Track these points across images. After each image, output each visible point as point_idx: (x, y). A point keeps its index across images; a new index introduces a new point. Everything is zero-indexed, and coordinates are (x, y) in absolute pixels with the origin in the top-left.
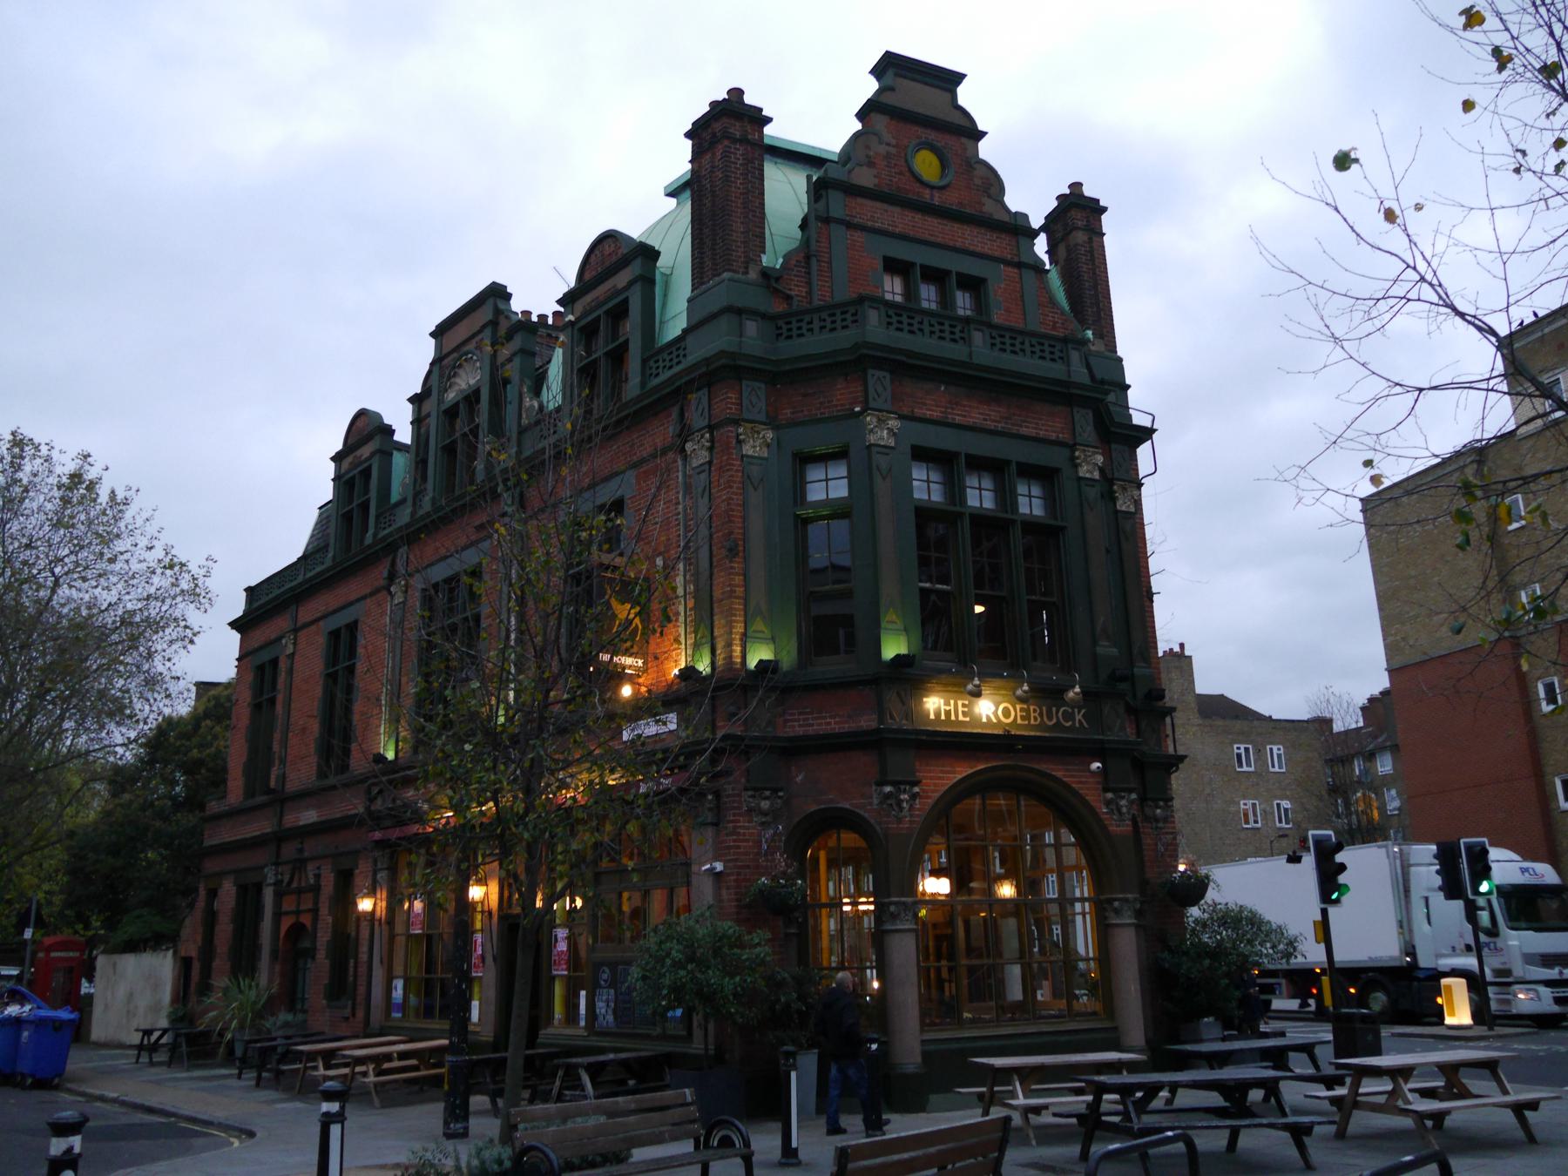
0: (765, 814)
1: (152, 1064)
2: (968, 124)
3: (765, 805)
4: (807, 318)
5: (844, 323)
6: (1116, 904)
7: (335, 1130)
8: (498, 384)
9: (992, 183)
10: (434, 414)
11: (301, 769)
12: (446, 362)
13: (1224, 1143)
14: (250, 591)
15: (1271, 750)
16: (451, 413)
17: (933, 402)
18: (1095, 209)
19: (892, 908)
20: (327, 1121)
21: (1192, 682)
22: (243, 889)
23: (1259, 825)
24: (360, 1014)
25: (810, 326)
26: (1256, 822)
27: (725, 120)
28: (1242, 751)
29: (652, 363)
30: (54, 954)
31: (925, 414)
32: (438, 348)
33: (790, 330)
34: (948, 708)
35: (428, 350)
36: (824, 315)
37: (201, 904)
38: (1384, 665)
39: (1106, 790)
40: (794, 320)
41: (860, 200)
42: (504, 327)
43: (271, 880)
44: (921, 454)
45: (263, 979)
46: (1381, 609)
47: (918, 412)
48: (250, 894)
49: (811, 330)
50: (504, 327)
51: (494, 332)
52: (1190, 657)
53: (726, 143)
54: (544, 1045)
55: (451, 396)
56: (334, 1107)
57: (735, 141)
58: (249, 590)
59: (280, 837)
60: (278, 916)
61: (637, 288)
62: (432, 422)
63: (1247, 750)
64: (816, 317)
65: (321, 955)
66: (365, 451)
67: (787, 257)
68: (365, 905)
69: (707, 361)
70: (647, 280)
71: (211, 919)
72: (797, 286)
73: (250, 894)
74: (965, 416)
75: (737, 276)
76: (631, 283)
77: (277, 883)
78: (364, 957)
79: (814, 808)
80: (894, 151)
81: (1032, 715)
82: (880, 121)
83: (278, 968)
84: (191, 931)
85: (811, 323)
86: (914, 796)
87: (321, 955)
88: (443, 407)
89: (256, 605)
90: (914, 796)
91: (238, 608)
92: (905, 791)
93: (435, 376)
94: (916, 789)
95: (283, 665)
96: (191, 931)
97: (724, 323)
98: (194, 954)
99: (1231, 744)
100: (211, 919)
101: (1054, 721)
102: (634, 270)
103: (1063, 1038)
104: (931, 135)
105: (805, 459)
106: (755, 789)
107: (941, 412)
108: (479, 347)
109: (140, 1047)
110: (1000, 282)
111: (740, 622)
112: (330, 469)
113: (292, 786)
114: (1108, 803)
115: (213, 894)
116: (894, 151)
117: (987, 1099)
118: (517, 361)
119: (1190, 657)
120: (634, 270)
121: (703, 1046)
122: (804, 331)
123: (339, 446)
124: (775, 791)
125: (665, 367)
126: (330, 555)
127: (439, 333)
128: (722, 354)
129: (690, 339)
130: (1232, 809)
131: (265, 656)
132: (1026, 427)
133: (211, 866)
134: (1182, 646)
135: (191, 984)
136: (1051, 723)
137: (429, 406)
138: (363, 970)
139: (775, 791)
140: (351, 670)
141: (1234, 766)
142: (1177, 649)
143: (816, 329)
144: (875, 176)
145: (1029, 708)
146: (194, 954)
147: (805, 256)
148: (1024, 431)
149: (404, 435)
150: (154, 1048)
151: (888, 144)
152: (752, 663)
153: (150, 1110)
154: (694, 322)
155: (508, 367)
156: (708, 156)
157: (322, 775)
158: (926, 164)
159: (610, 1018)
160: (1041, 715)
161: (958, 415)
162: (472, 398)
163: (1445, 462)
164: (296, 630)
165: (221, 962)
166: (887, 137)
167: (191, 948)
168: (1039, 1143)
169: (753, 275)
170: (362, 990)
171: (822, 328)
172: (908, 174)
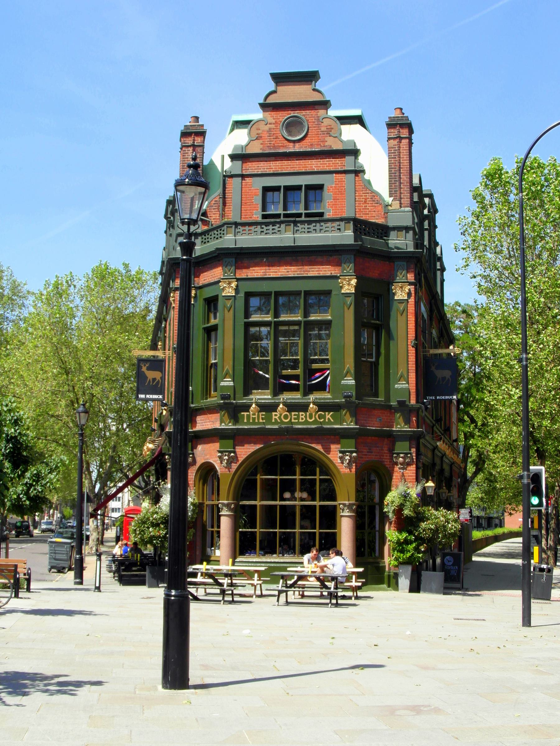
5: (250, 232)
25: (279, 229)
31: (254, 275)
34: (254, 416)
72: (215, 214)
74: (276, 272)
80: (273, 126)
81: (301, 417)
92: (226, 455)
101: (313, 419)
107: (263, 272)
111: (410, 329)
125: (214, 237)
132: (312, 271)
136: (311, 421)
143: (318, 230)
144: (262, 144)
145: (299, 414)
151: (270, 124)
160: (306, 417)
161: (273, 272)
163: (389, 301)
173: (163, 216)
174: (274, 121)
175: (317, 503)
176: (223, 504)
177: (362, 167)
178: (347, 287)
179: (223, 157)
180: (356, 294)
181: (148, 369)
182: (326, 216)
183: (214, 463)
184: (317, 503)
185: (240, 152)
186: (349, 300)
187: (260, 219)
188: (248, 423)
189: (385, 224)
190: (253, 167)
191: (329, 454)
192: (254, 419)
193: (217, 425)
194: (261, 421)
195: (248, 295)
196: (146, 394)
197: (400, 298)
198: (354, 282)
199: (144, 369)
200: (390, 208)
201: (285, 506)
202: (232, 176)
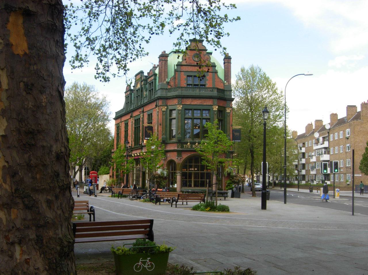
0: (164, 160)
1: (107, 192)
2: (205, 49)
8: (142, 88)
17: (188, 102)
47: (186, 104)
52: (357, 107)
58: (116, 113)
71: (113, 169)
80: (190, 56)
84: (111, 171)
94: (181, 157)
98: (111, 175)
102: (153, 78)
116: (190, 56)
119: (357, 107)
120: (153, 78)
121: (352, 203)
123: (125, 91)
127: (136, 76)
140: (127, 130)
146: (111, 175)
147: (174, 78)
148: (204, 104)
168: (191, 179)
169: (165, 82)
172: (192, 60)
173: (135, 75)
174: (190, 55)
175: (199, 172)
176: (178, 172)
177: (217, 71)
178: (215, 109)
179: (175, 65)
180: (217, 111)
181: (148, 130)
182: (207, 86)
183: (175, 160)
184: (199, 172)
185: (179, 64)
186: (216, 112)
187: (186, 86)
188: (186, 148)
189: (224, 89)
190: (184, 69)
191: (311, 171)
192: (187, 147)
193: (176, 148)
194: (189, 147)
195: (186, 109)
196: (147, 138)
197: (228, 112)
198: (217, 107)
199: (147, 130)
200: (225, 84)
201: (202, 173)
202: (177, 71)
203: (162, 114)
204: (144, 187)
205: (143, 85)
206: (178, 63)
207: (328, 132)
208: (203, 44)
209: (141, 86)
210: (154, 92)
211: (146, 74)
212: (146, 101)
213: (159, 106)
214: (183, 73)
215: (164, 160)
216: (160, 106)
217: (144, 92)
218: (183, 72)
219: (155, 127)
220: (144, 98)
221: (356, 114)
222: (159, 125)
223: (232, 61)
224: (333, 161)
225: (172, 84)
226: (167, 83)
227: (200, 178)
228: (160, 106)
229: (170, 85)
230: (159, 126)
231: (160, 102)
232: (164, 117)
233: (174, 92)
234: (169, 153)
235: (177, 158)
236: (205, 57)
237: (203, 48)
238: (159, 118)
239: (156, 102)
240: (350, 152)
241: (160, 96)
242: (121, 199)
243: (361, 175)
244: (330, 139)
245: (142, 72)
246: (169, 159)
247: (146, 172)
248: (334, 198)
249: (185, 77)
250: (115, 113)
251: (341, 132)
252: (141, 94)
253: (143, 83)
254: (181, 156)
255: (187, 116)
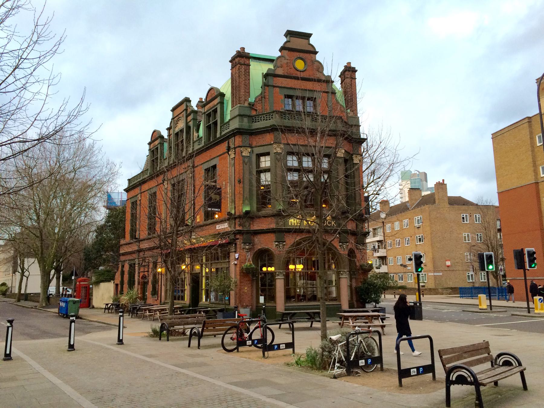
0: (247, 249)
1: (109, 313)
2: (314, 50)
3: (247, 247)
4: (260, 116)
6: (341, 272)
7: (122, 318)
8: (188, 128)
9: (320, 67)
10: (173, 134)
11: (143, 233)
12: (175, 119)
13: (310, 326)
14: (129, 180)
15: (476, 216)
16: (177, 134)
17: (293, 139)
18: (354, 71)
19: (277, 273)
20: (120, 316)
21: (447, 193)
22: (131, 266)
23: (470, 242)
24: (159, 299)
26: (468, 240)
27: (238, 58)
28: (465, 216)
29: (223, 127)
30: (81, 283)
32: (173, 115)
33: (256, 120)
35: (170, 115)
36: (264, 116)
37: (120, 269)
38: (497, 191)
39: (340, 242)
40: (257, 117)
41: (278, 78)
42: (189, 111)
43: (137, 262)
44: (291, 153)
45: (136, 289)
46: (496, 172)
48: (132, 266)
49: (261, 120)
50: (189, 111)
51: (186, 113)
52: (446, 184)
53: (239, 65)
54: (199, 307)
55: (177, 130)
56: (121, 314)
57: (241, 64)
58: (129, 180)
59: (139, 251)
60: (139, 273)
61: (219, 105)
62: (172, 136)
63: (466, 216)
64: (262, 116)
65: (150, 283)
66: (157, 142)
67: (256, 98)
68: (159, 270)
69: (233, 130)
70: (222, 103)
71: (123, 273)
73: (132, 266)
75: (242, 105)
76: (217, 104)
77: (139, 264)
78: (160, 284)
79: (260, 248)
80: (289, 61)
82: (286, 52)
83: (140, 287)
85: (261, 118)
86: (284, 245)
87: (150, 283)
88: (175, 132)
89: (131, 184)
90: (284, 245)
91: (126, 185)
93: (172, 124)
94: (284, 243)
95: (138, 203)
96: (118, 276)
97: (237, 119)
99: (460, 214)
100: (123, 273)
102: (218, 100)
103: (310, 307)
104: (301, 55)
105: (259, 156)
106: (245, 243)
108: (183, 116)
109: (105, 309)
110: (321, 98)
112: (147, 147)
113: (142, 238)
114: (340, 246)
115: (123, 266)
116: (289, 61)
117: (342, 324)
118: (192, 122)
119: (446, 184)
120: (218, 100)
122: (259, 120)
123: (149, 140)
124: (250, 243)
126: (149, 172)
127: (173, 110)
128: (236, 129)
129: (231, 122)
130: (460, 236)
131: (133, 200)
133: (122, 258)
134: (443, 180)
135: (119, 290)
137: (172, 131)
138: (160, 287)
139: (250, 243)
141: (461, 221)
142: (441, 181)
143: (262, 120)
146: (119, 283)
147: (262, 97)
149: (166, 137)
150: (109, 309)
152: (244, 211)
153: (105, 323)
154: (233, 116)
155: (190, 123)
156: (234, 69)
157: (149, 234)
158: (300, 65)
159: (214, 299)
162: (182, 131)
164: (141, 193)
165: (126, 286)
166: (287, 57)
167: (118, 281)
169: (246, 104)
170: (159, 292)
171: (264, 119)
172: (293, 68)
197: (356, 162)
202: (268, 86)
203: (242, 162)
204: (198, 304)
205: (190, 121)
206: (268, 71)
207: (383, 222)
208: (311, 42)
209: (187, 123)
210: (221, 127)
211: (194, 104)
212: (197, 147)
213: (235, 148)
214: (277, 89)
215: (247, 249)
216: (239, 147)
217: (195, 133)
218: (277, 88)
219: (226, 188)
220: (193, 143)
221: (421, 198)
222: (237, 182)
223: (357, 75)
224: (526, 250)
225: (259, 107)
226: (249, 104)
227: (187, 281)
228: (239, 147)
229: (256, 110)
230: (237, 184)
231: (238, 140)
232: (246, 167)
233: (265, 122)
234: (259, 236)
235: (277, 245)
236: (315, 65)
237: (310, 49)
238: (237, 170)
239: (227, 141)
240: (423, 245)
241: (238, 127)
242: (168, 340)
243: (441, 274)
244: (386, 230)
245: (187, 100)
246: (259, 247)
247: (202, 274)
248: (529, 312)
249: (283, 97)
250: (127, 182)
251: (406, 221)
252: (187, 138)
253: (190, 118)
254: (284, 242)
255: (305, 159)
